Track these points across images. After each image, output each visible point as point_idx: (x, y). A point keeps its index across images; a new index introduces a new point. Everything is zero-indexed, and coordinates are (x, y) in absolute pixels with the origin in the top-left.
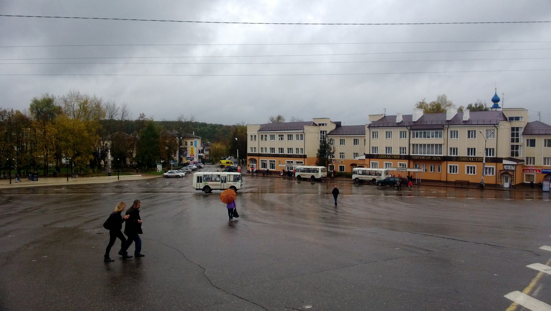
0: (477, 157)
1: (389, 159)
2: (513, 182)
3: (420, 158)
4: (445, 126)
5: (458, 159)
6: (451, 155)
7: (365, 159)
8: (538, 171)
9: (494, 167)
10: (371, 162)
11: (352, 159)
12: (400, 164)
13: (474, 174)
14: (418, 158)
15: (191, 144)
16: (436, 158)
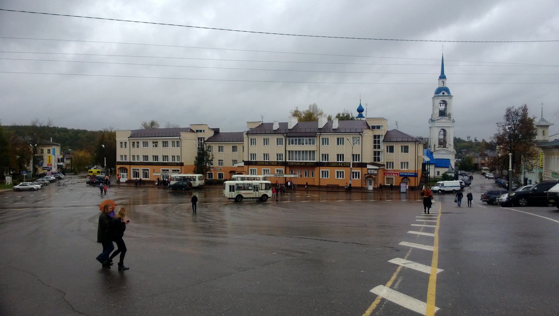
1: (341, 166)
2: (376, 185)
3: (295, 164)
5: (329, 165)
7: (243, 165)
9: (360, 171)
10: (249, 168)
13: (359, 178)
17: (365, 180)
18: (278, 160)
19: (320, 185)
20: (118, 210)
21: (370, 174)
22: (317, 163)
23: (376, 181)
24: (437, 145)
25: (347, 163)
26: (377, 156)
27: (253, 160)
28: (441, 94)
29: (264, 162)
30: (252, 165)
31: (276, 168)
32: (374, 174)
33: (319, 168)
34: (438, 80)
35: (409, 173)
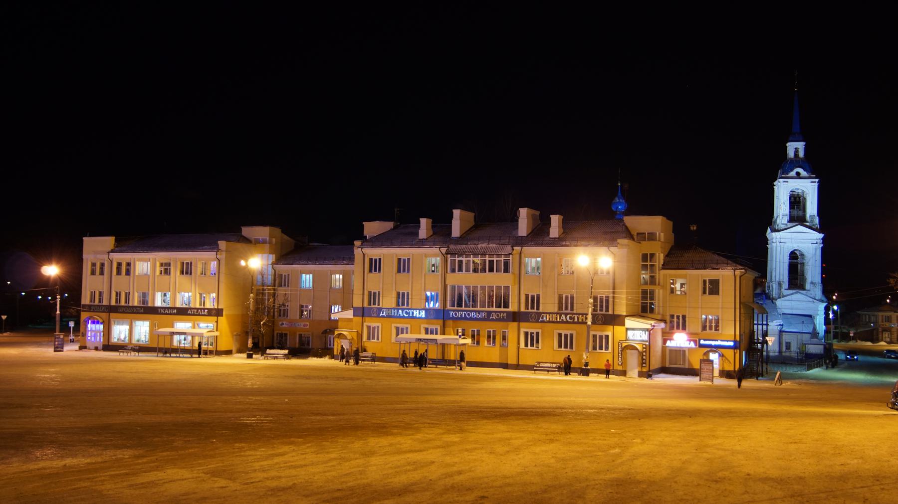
2: (644, 365)
7: (352, 317)
9: (380, 325)
10: (365, 324)
14: (461, 315)
15: (652, 298)
17: (622, 353)
19: (520, 363)
20: (39, 465)
23: (644, 357)
24: (785, 285)
25: (581, 316)
26: (649, 301)
27: (530, 310)
30: (527, 321)
31: (441, 327)
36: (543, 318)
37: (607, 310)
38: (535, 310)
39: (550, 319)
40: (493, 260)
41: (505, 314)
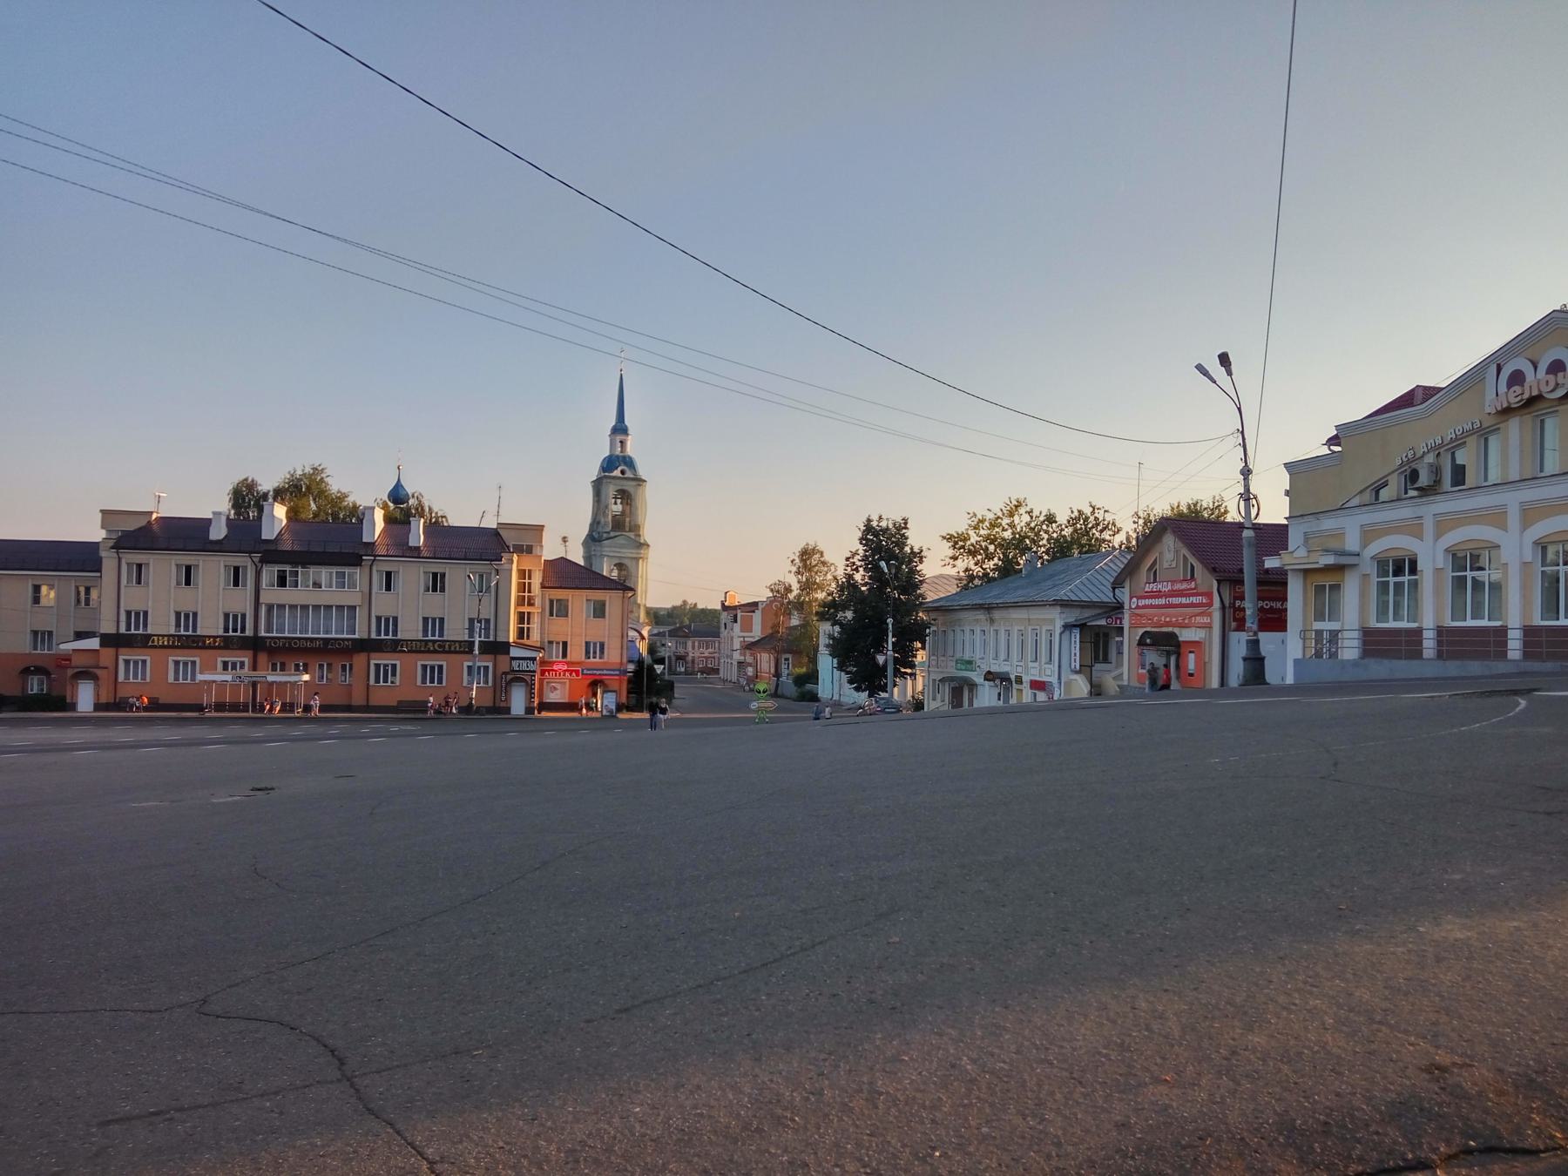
0: (448, 641)
1: (435, 652)
3: (290, 644)
4: (364, 558)
5: (395, 646)
6: (380, 635)
8: (574, 674)
9: (490, 665)
11: (27, 652)
12: (1114, 678)
13: (441, 683)
16: (339, 644)
17: (506, 688)
18: (226, 630)
21: (517, 671)
22: (361, 641)
27: (383, 637)
28: (617, 473)
29: (426, 645)
32: (527, 671)
33: (369, 656)
34: (610, 435)
35: (607, 670)
36: (153, 641)
37: (243, 630)
38: (390, 637)
39: (163, 642)
40: (1466, 576)
41: (321, 642)
